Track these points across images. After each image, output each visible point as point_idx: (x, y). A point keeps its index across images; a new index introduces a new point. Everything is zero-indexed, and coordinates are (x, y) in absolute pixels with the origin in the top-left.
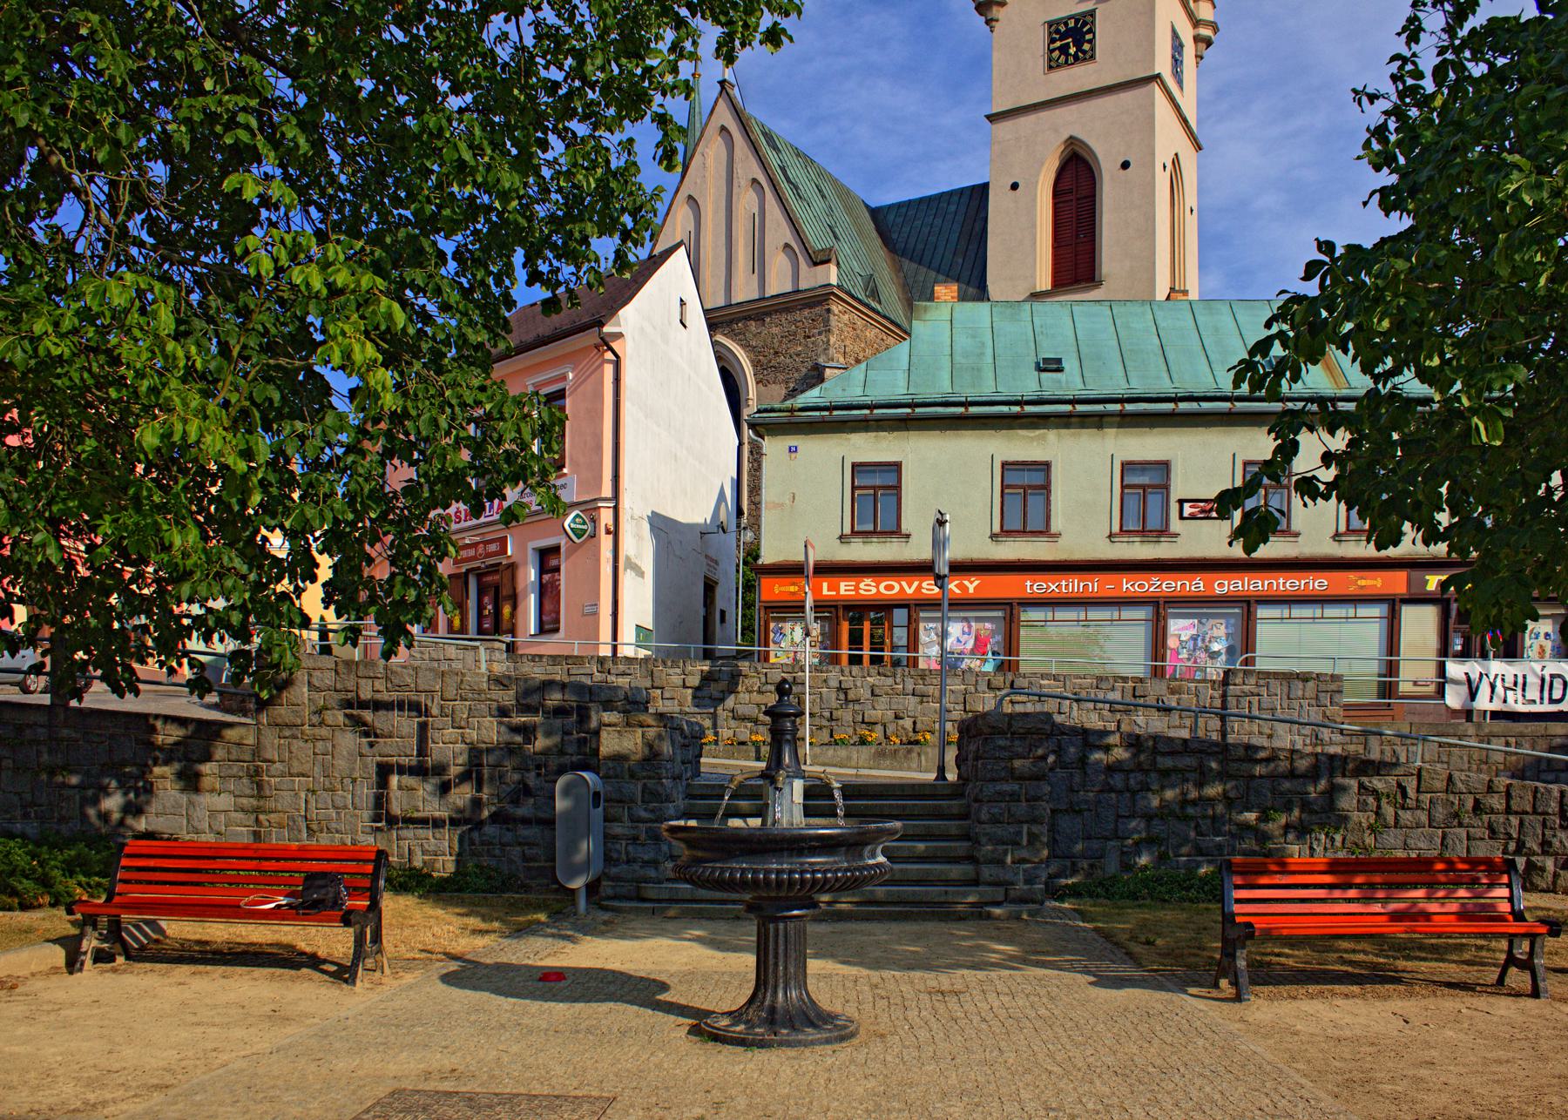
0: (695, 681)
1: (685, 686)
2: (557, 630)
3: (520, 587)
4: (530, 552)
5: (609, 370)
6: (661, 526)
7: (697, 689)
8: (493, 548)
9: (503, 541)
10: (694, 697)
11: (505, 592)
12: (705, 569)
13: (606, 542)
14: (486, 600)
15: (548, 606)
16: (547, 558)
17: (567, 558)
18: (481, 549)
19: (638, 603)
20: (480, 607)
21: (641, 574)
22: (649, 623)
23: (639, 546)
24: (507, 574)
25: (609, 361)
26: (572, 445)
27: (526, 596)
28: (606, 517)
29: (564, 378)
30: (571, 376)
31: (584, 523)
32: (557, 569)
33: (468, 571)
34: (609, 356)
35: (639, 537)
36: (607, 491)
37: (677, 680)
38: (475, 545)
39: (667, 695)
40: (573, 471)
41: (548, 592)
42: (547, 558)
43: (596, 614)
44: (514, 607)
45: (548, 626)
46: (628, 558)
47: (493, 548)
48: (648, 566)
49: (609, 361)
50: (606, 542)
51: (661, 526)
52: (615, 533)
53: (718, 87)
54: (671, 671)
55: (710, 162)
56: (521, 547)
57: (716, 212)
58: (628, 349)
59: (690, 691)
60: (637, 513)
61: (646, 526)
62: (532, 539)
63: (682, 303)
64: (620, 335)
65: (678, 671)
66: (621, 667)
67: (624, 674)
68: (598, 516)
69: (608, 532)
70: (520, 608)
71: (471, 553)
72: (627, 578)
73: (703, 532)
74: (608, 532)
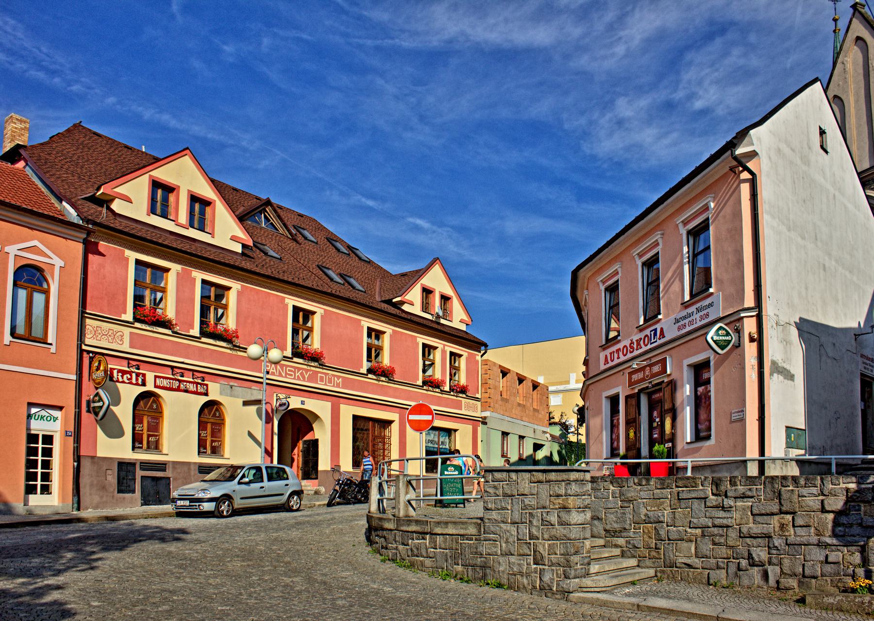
0: (837, 503)
1: (823, 510)
2: (708, 437)
3: (678, 402)
4: (685, 368)
5: (745, 188)
6: (809, 331)
7: (838, 514)
8: (656, 369)
9: (663, 362)
10: (836, 523)
11: (667, 406)
12: (861, 367)
13: (750, 350)
14: (655, 414)
15: (703, 416)
16: (700, 370)
17: (715, 372)
18: (647, 372)
19: (789, 404)
20: (651, 420)
21: (791, 377)
22: (800, 422)
23: (786, 350)
24: (667, 391)
25: (745, 181)
26: (717, 266)
27: (683, 409)
28: (749, 326)
29: (706, 208)
30: (712, 205)
31: (728, 334)
32: (708, 382)
33: (640, 391)
34: (745, 175)
35: (786, 342)
36: (749, 302)
37: (813, 502)
38: (642, 369)
39: (800, 521)
40: (718, 290)
41: (701, 402)
42: (700, 370)
43: (742, 420)
44: (674, 420)
45: (701, 435)
46: (774, 363)
47: (656, 369)
48: (798, 368)
49: (745, 181)
50: (750, 350)
51: (809, 331)
52: (759, 340)
53: (851, 11)
54: (805, 491)
55: (849, 66)
56: (678, 366)
57: (857, 101)
58: (761, 166)
59: (831, 516)
60: (783, 319)
61: (794, 332)
62: (688, 357)
63: (822, 132)
64: (753, 154)
65: (814, 490)
66: (741, 489)
67: (744, 497)
68: (742, 327)
69: (752, 340)
70: (679, 420)
71: (640, 375)
72: (773, 383)
73: (857, 335)
74: (752, 340)
